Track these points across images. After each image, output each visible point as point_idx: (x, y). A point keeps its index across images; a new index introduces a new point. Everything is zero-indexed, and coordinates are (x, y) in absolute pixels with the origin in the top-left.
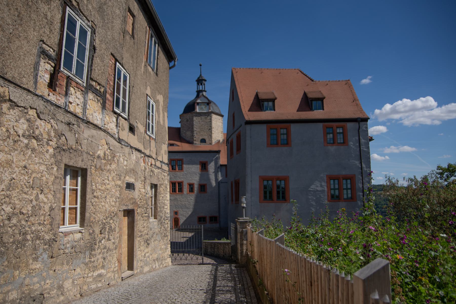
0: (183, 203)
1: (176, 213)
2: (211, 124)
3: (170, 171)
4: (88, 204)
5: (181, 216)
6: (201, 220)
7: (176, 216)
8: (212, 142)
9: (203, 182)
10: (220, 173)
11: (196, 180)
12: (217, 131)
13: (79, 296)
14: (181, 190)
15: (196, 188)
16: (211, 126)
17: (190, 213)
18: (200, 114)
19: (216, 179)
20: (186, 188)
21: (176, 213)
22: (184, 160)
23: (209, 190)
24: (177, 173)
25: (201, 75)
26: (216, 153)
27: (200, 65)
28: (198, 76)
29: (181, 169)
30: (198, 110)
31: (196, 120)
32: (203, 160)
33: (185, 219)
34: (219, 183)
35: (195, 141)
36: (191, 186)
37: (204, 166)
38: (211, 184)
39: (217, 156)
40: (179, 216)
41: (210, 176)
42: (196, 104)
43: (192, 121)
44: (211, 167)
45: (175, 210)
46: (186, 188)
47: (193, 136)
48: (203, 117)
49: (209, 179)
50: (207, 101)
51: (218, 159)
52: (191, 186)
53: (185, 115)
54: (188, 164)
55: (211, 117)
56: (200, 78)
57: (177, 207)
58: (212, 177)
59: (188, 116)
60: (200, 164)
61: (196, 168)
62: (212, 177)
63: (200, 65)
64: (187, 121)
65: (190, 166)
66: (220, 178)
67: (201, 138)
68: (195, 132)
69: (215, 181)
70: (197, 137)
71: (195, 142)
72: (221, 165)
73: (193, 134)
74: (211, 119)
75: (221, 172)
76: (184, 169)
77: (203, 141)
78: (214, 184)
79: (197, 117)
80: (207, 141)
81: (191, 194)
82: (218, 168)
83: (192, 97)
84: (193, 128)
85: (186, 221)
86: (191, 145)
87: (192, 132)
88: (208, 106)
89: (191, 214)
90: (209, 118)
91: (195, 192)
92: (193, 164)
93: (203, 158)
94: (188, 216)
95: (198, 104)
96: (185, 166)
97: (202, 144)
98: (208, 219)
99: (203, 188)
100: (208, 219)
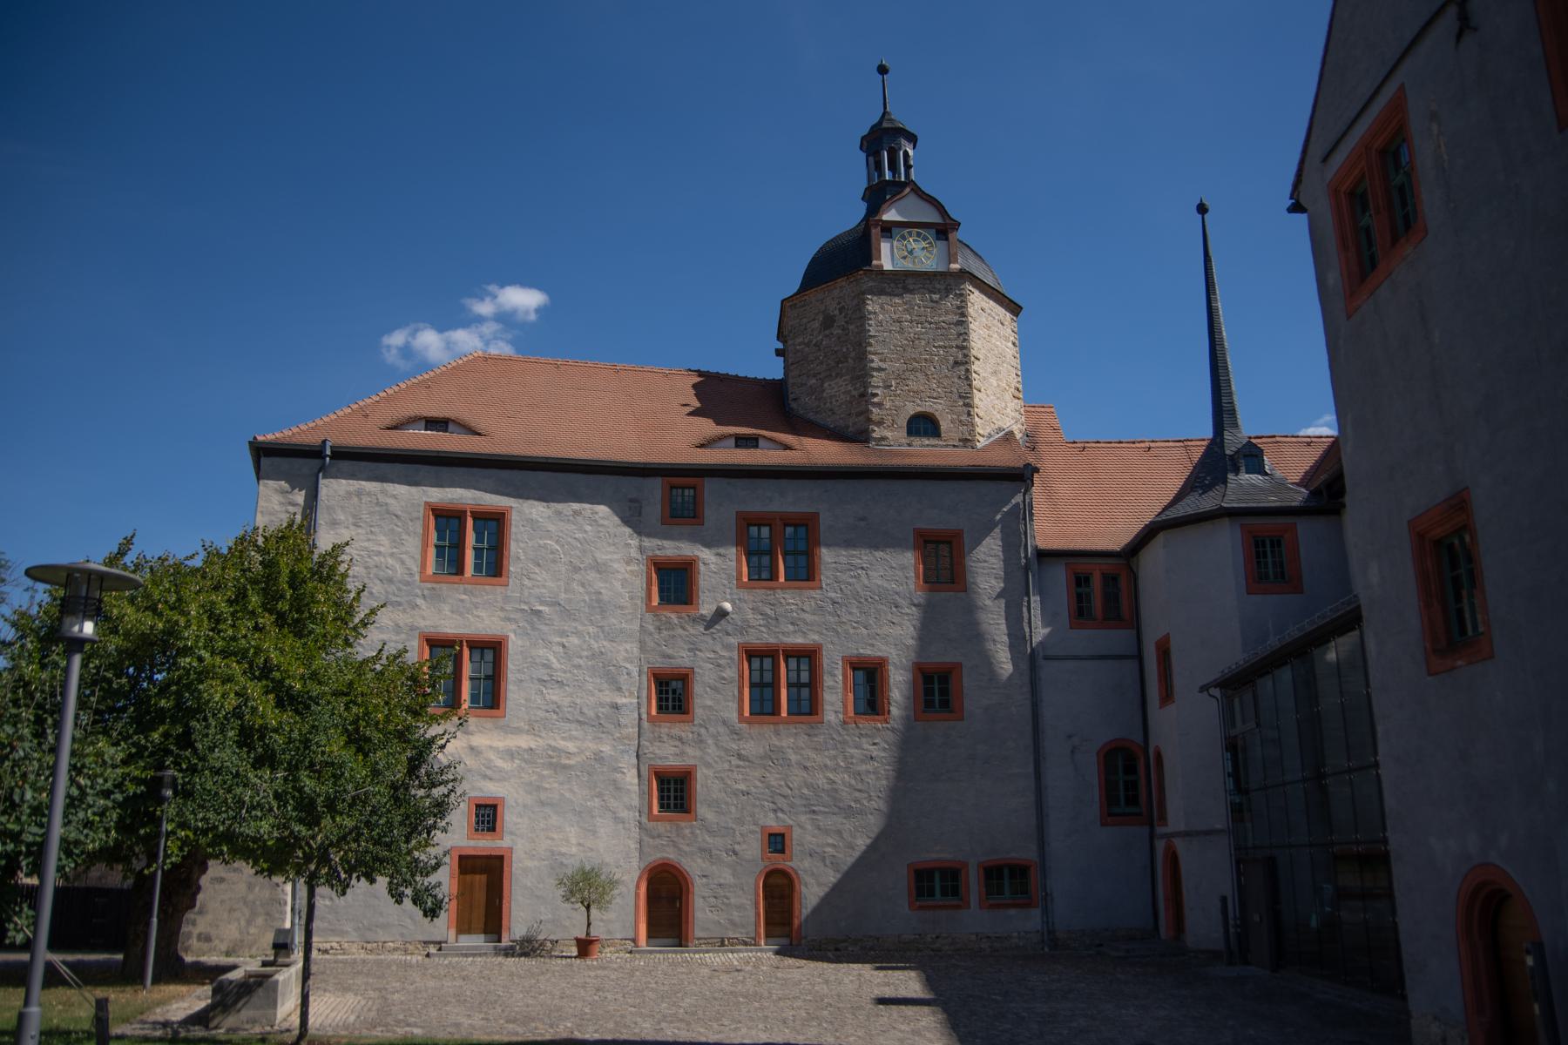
0: (821, 781)
1: (777, 842)
2: (964, 335)
3: (740, 585)
4: (301, 461)
5: (807, 864)
6: (935, 883)
7: (779, 861)
8: (972, 431)
9: (941, 656)
10: (1035, 600)
11: (895, 640)
12: (993, 381)
13: (624, 912)
14: (808, 705)
15: (898, 686)
16: (964, 348)
17: (862, 842)
18: (901, 282)
19: (1017, 637)
20: (836, 693)
21: (777, 842)
22: (825, 521)
23: (973, 696)
24: (780, 594)
25: (885, 113)
26: (1006, 485)
27: (883, 70)
28: (876, 120)
29: (805, 572)
30: (887, 257)
31: (880, 311)
32: (935, 519)
33: (832, 878)
34: (1032, 661)
35: (880, 423)
36: (869, 675)
37: (943, 562)
38: (987, 661)
39: (1018, 498)
40: (798, 863)
41: (983, 617)
42: (875, 232)
43: (860, 317)
44: (987, 564)
45: (772, 822)
46: (836, 693)
47: (865, 396)
48: (917, 299)
49: (975, 637)
50: (932, 217)
51: (1024, 514)
52: (869, 675)
53: (813, 295)
54: (849, 544)
55: (962, 297)
56: (885, 125)
57: (782, 802)
58: (994, 623)
59: (836, 294)
60: (915, 548)
61: (894, 573)
62: (994, 623)
63: (883, 70)
64: (829, 322)
65: (862, 557)
66: (1040, 632)
67: (912, 409)
68: (876, 379)
69: (1012, 647)
70: (892, 408)
71: (877, 432)
72: (1043, 555)
73: (866, 385)
74: (962, 312)
75: (1041, 593)
76: (826, 576)
77: (924, 425)
78: (1004, 663)
79: (884, 299)
80: (944, 425)
81: (867, 724)
82: (1027, 568)
83: (851, 214)
84: (862, 357)
85: (836, 889)
86: (859, 446)
87: (861, 374)
88: (941, 244)
89: (872, 848)
90: (950, 302)
91: (895, 711)
92: (875, 546)
93: (938, 510)
94: (849, 859)
95: (888, 229)
96: (826, 555)
97: (917, 441)
98: (973, 883)
99: (937, 687)
100: (973, 883)
